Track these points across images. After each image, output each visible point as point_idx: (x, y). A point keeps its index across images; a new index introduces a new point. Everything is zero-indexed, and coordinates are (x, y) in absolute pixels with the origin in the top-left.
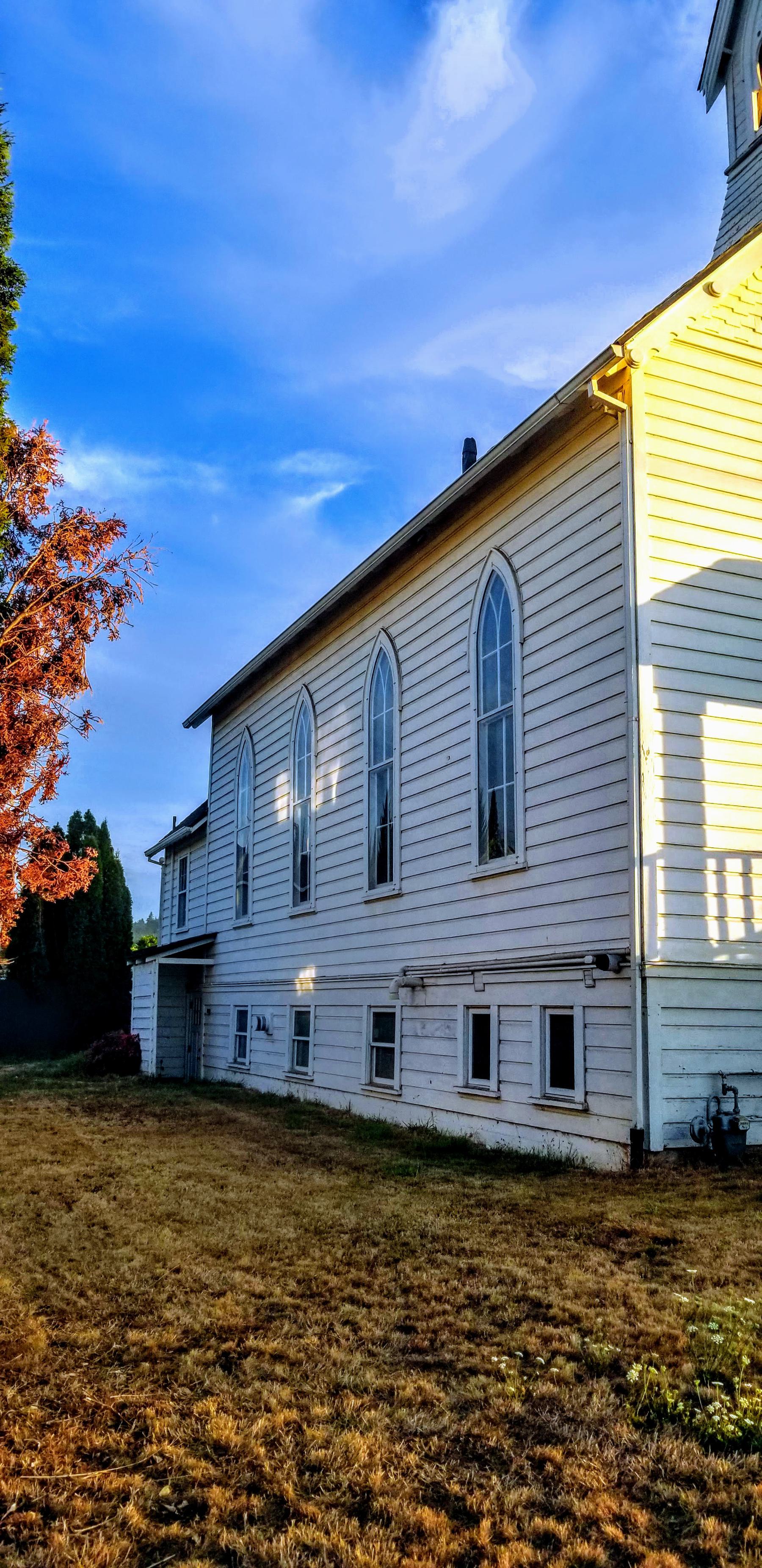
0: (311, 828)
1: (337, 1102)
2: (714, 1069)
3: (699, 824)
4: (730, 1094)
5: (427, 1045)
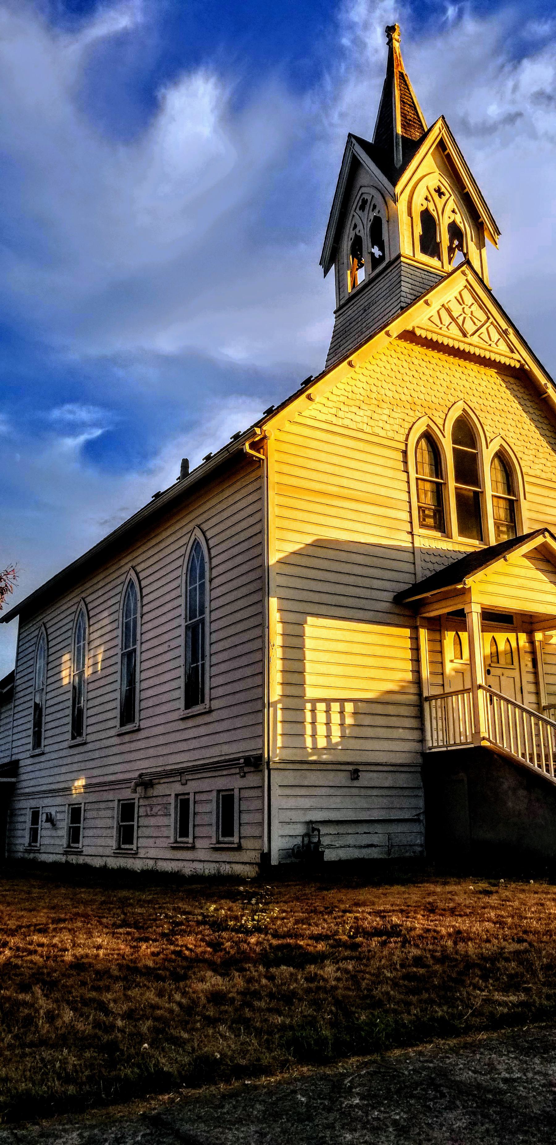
0: (84, 690)
1: (97, 862)
2: (308, 818)
3: (302, 684)
4: (316, 833)
5: (152, 821)
